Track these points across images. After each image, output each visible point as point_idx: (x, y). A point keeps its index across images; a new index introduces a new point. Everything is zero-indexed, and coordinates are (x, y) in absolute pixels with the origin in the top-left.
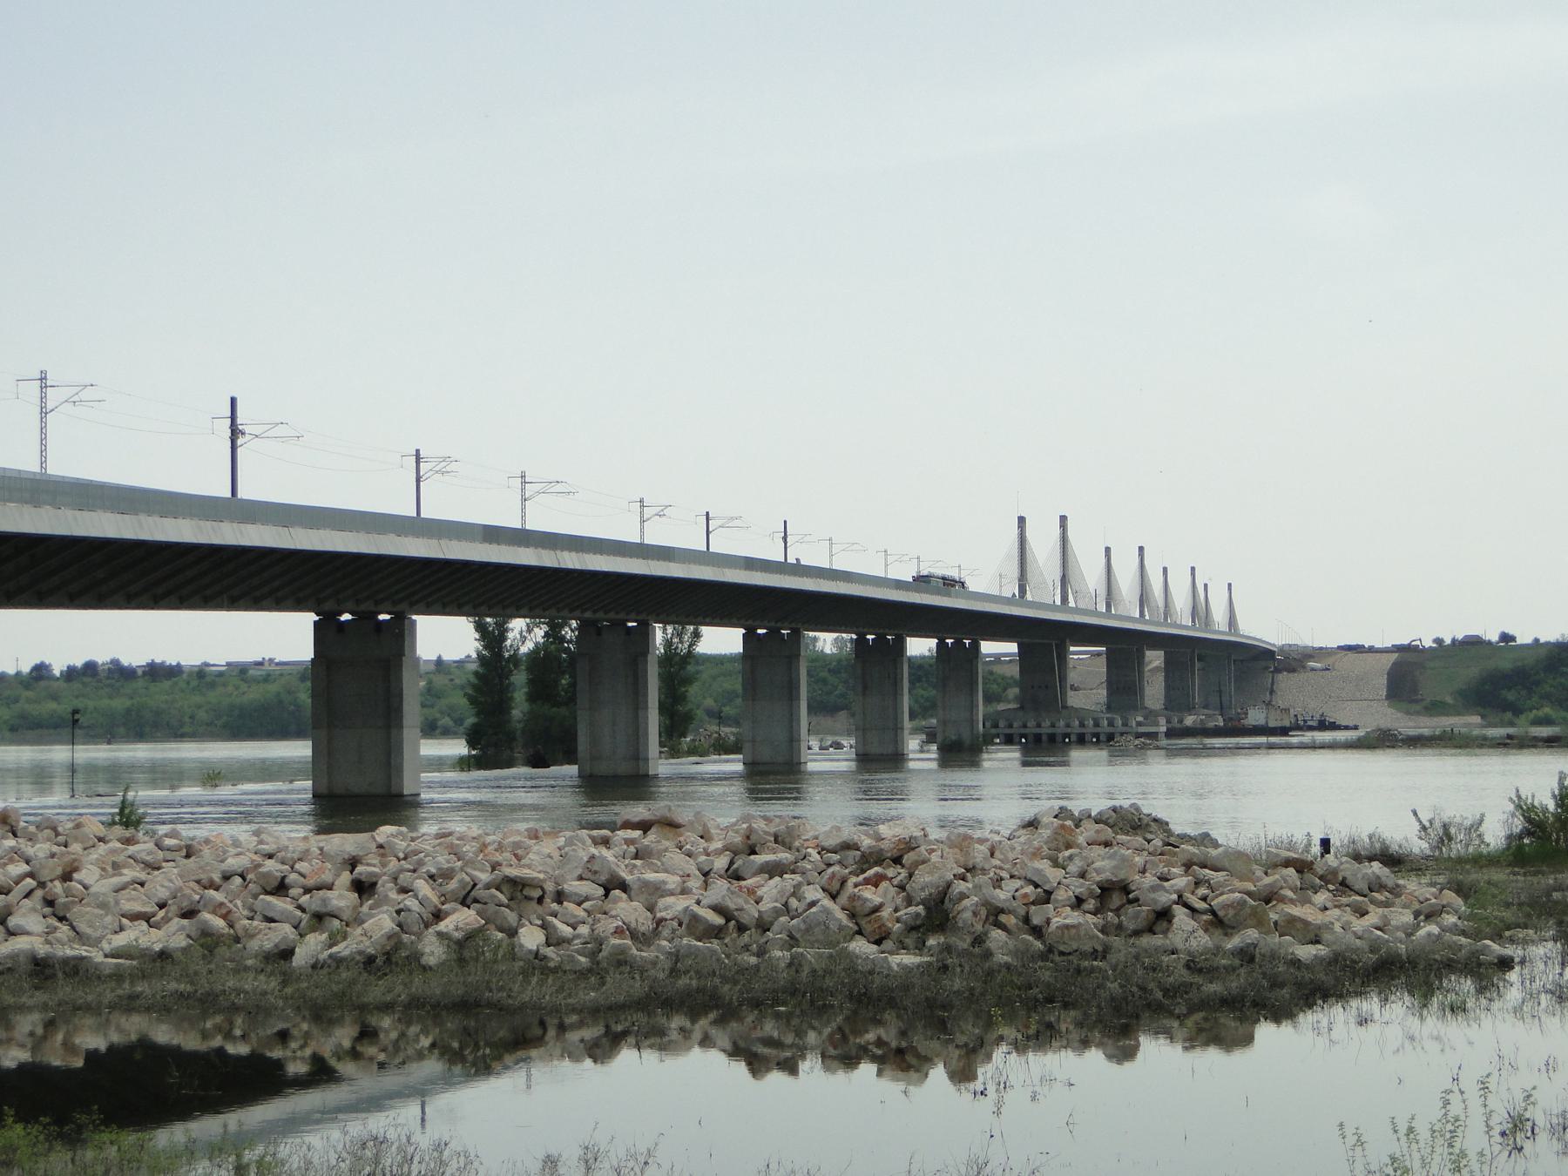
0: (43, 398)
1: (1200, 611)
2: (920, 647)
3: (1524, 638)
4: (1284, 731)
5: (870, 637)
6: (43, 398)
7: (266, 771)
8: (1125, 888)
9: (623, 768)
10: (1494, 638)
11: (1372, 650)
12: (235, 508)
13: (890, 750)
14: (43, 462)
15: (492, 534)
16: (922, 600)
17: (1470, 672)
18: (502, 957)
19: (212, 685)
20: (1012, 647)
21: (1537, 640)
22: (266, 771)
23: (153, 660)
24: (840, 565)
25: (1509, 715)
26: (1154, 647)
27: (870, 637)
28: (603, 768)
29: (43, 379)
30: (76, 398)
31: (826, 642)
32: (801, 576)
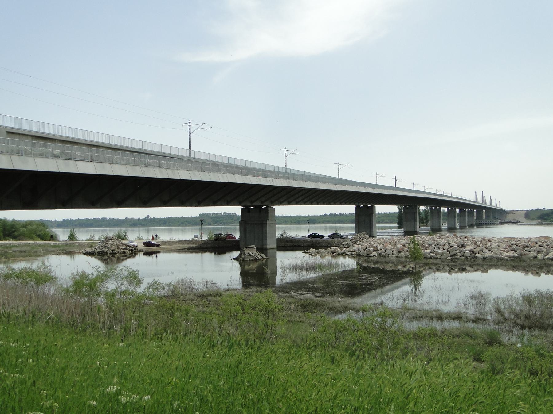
0: (286, 153)
1: (484, 201)
2: (444, 209)
3: (547, 209)
4: (514, 223)
5: (433, 207)
6: (286, 153)
7: (390, 228)
8: (416, 302)
9: (437, 228)
10: (542, 209)
11: (521, 211)
12: (395, 188)
13: (464, 225)
14: (339, 176)
15: (434, 194)
16: (307, 186)
17: (539, 214)
18: (82, 374)
19: (349, 216)
20: (236, 210)
21: (55, 220)
22: (390, 228)
23: (235, 213)
24: (427, 191)
25: (545, 220)
26: (484, 210)
27: (433, 207)
28: (434, 228)
29: (189, 123)
30: (293, 153)
31: (422, 208)
32: (398, 190)
